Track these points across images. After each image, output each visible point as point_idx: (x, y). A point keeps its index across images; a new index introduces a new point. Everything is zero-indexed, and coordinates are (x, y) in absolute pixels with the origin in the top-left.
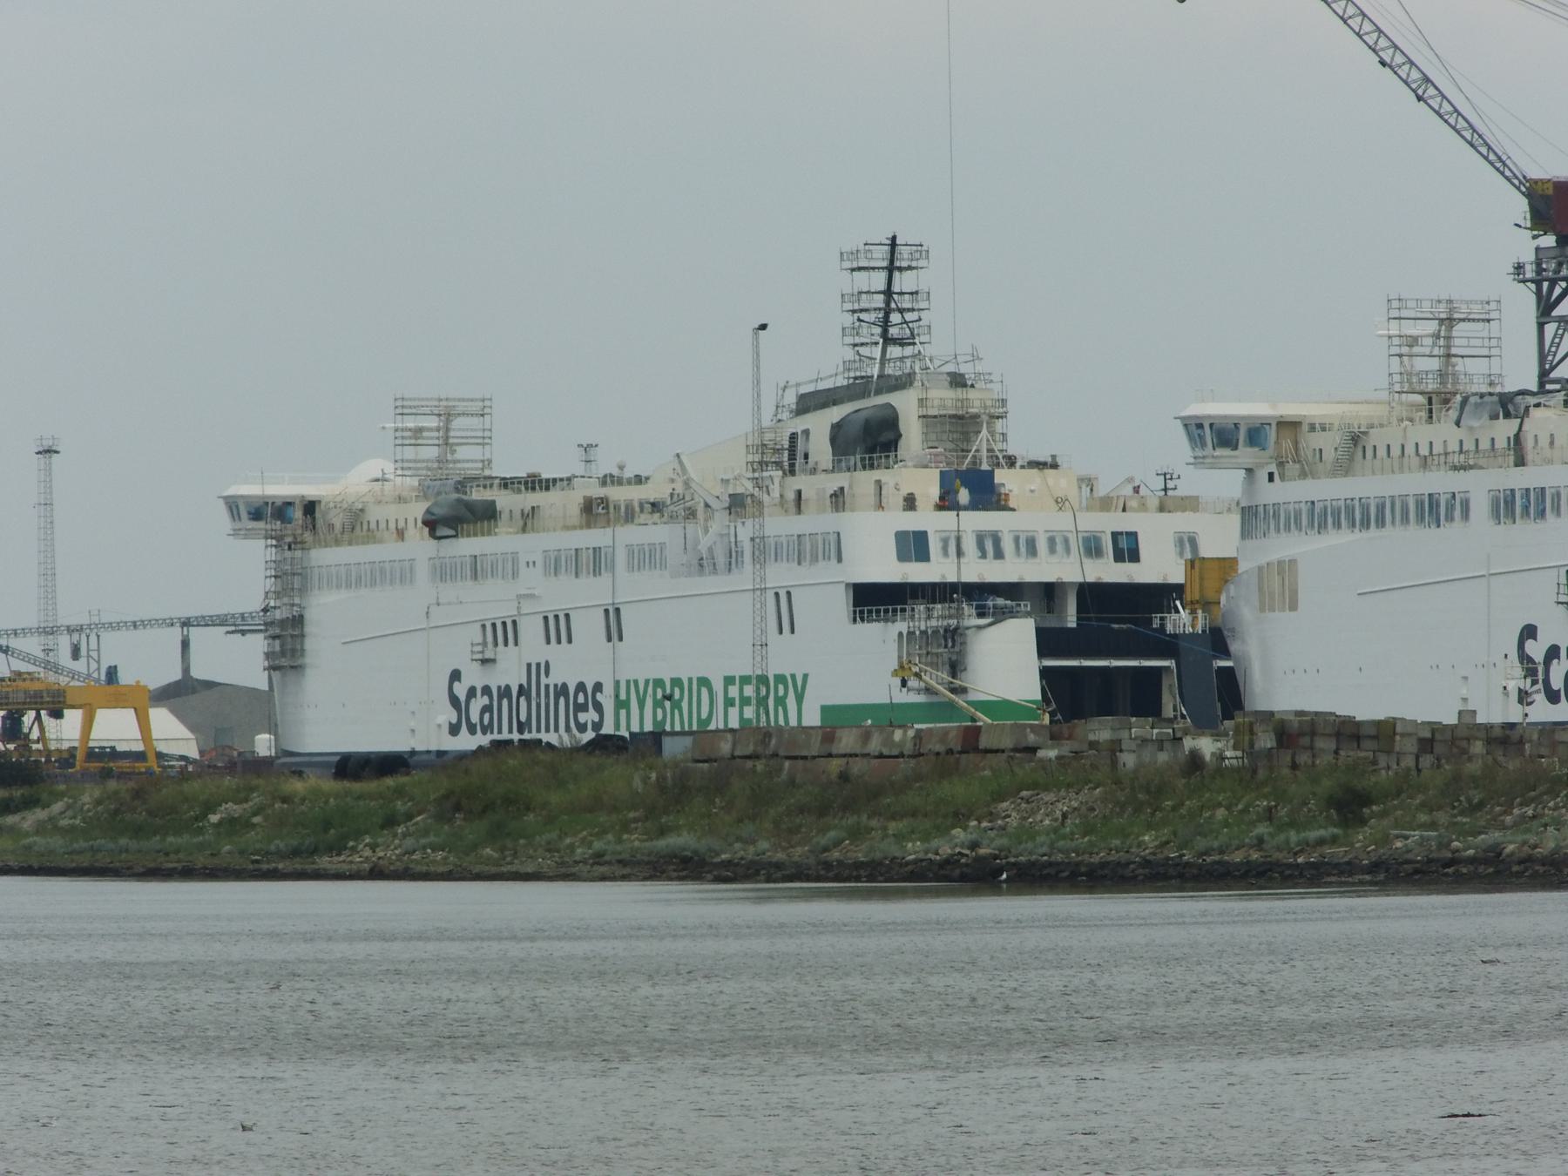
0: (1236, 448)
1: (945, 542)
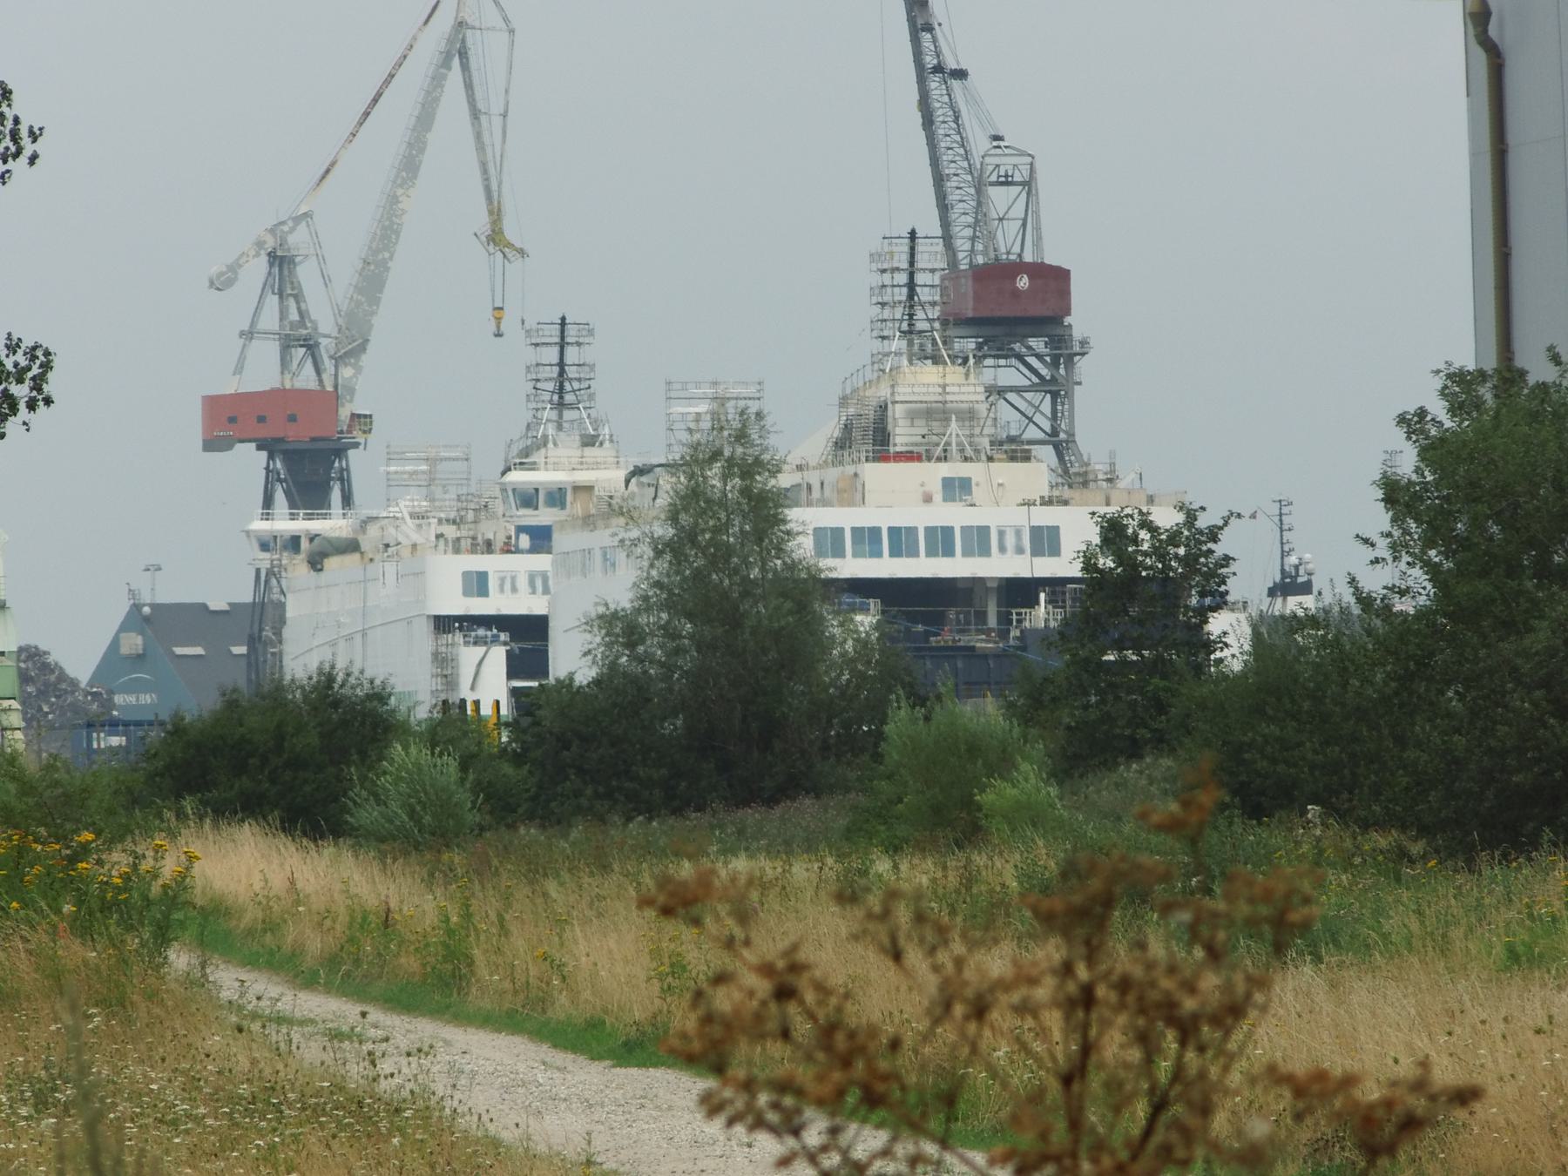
0: (536, 508)
1: (503, 580)
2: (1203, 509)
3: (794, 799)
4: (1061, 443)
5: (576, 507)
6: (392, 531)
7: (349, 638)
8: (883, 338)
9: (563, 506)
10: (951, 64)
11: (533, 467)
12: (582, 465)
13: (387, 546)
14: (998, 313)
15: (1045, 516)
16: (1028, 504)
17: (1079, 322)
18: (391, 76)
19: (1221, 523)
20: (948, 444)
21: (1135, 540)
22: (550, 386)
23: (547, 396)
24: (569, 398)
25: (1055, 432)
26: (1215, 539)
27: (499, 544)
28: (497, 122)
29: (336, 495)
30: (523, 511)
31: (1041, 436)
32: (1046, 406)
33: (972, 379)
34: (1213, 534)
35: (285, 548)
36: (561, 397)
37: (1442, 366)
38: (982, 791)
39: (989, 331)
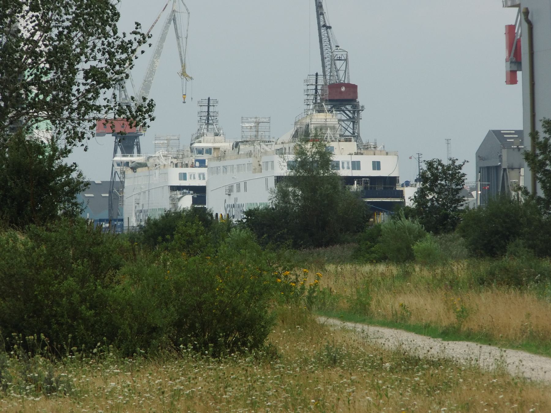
1: (191, 175)
2: (457, 159)
3: (333, 245)
4: (355, 136)
5: (214, 154)
6: (158, 160)
7: (144, 192)
8: (308, 105)
9: (210, 153)
10: (328, 25)
11: (200, 142)
12: (215, 142)
13: (156, 165)
14: (336, 98)
15: (356, 158)
16: (351, 154)
17: (361, 99)
18: (153, 26)
19: (462, 164)
20: (327, 136)
21: (437, 169)
22: (205, 118)
23: (204, 121)
24: (210, 122)
25: (354, 133)
26: (461, 169)
27: (190, 164)
28: (184, 40)
29: (135, 150)
30: (198, 155)
31: (350, 134)
32: (351, 126)
33: (334, 117)
34: (460, 167)
35: (124, 165)
36: (208, 121)
37: (542, 119)
38: (413, 245)
39: (334, 103)
